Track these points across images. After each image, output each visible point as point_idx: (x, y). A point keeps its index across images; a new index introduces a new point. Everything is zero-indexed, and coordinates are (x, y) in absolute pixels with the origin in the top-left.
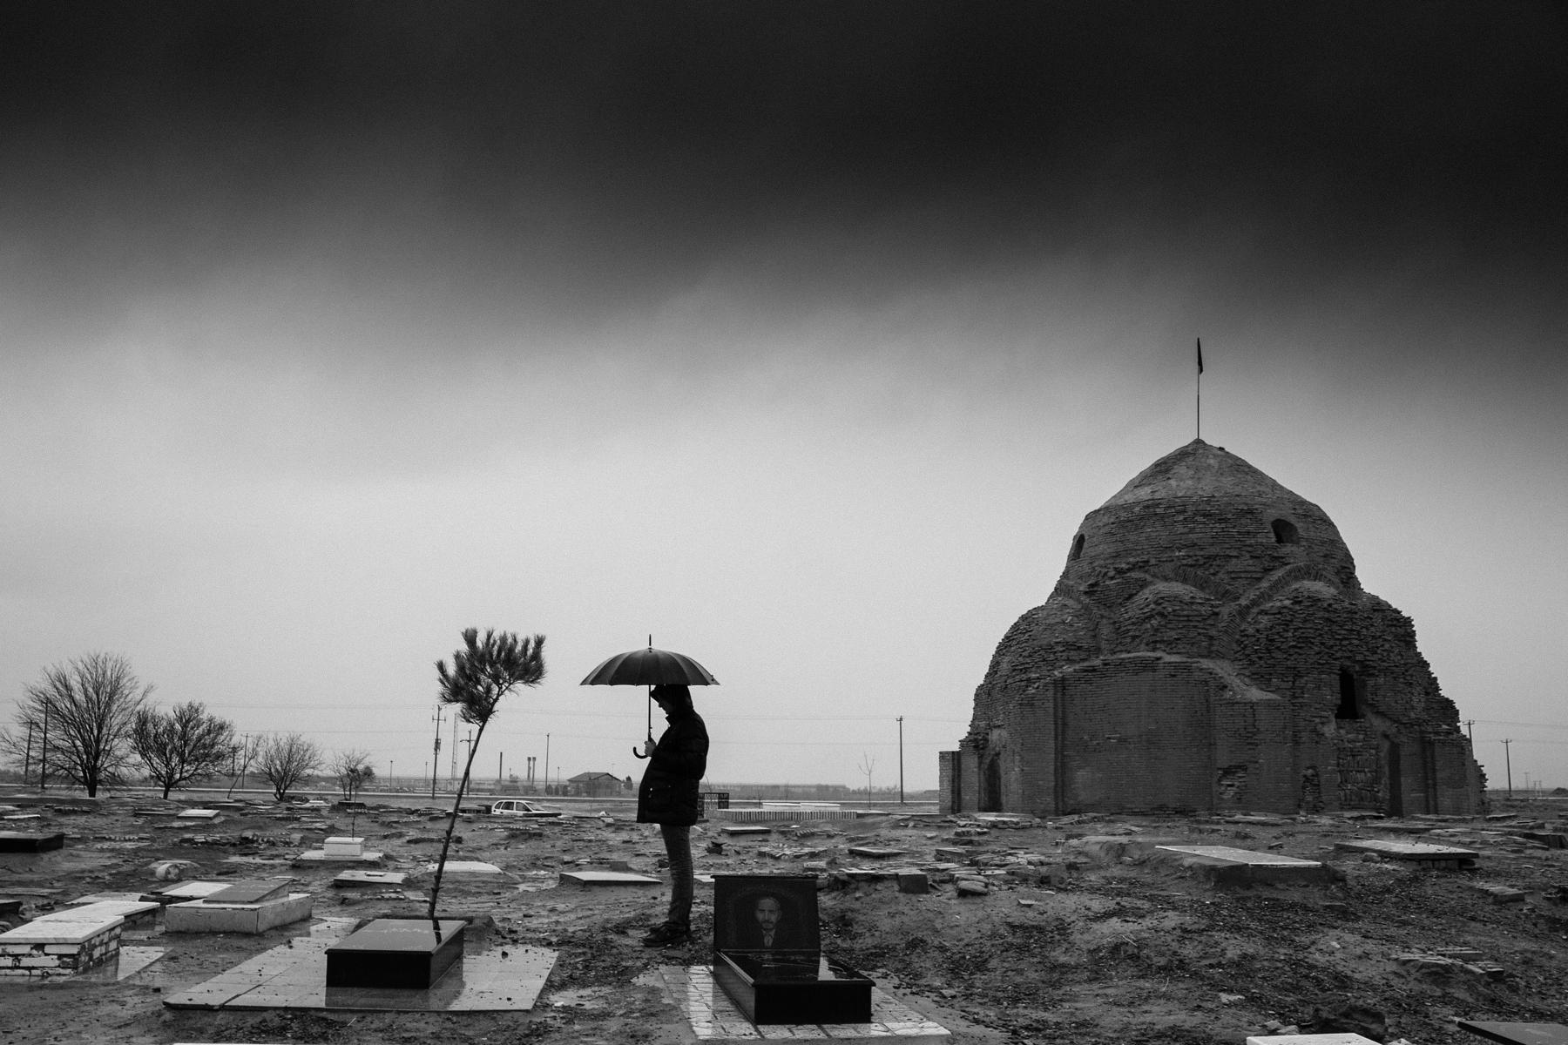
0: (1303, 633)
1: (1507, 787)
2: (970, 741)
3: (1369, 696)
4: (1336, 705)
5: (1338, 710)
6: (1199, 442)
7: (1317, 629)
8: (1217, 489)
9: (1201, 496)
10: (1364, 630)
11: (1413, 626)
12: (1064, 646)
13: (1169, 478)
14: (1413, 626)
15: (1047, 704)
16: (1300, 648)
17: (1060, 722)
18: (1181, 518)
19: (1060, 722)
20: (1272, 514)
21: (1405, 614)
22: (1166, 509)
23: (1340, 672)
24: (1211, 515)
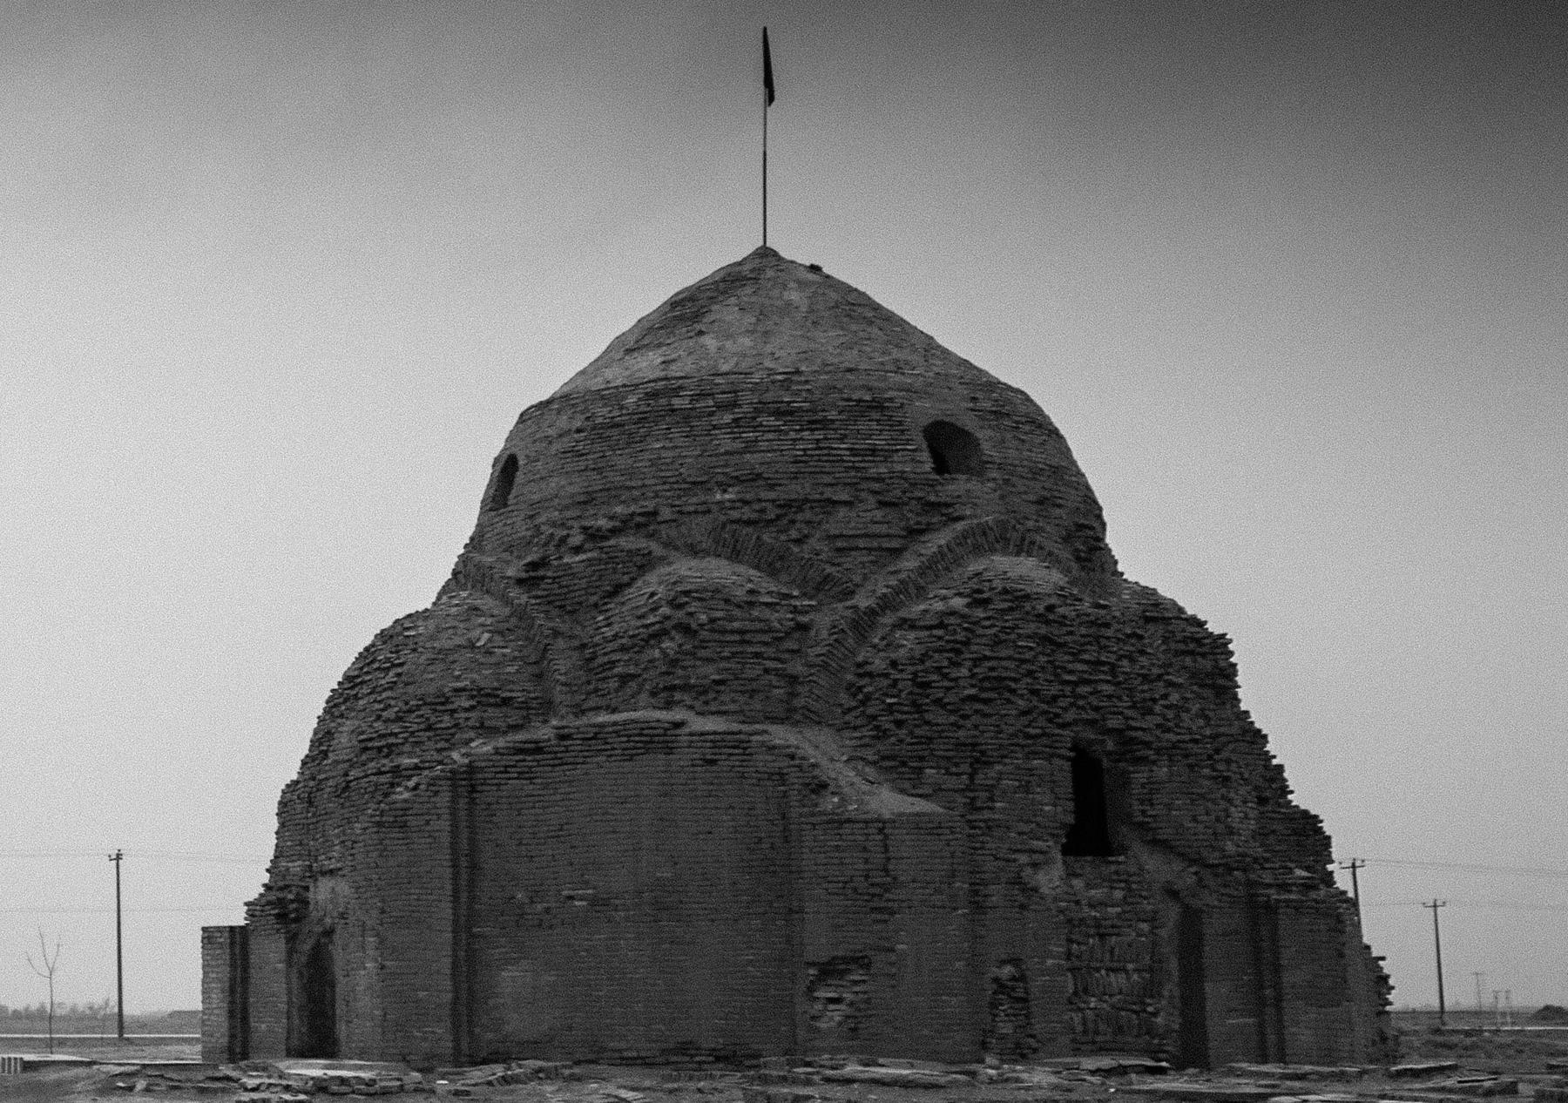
0: (992, 669)
3: (1137, 807)
6: (765, 254)
9: (771, 372)
10: (1125, 662)
12: (473, 697)
13: (701, 333)
16: (986, 701)
17: (464, 862)
18: (728, 418)
19: (464, 862)
20: (925, 411)
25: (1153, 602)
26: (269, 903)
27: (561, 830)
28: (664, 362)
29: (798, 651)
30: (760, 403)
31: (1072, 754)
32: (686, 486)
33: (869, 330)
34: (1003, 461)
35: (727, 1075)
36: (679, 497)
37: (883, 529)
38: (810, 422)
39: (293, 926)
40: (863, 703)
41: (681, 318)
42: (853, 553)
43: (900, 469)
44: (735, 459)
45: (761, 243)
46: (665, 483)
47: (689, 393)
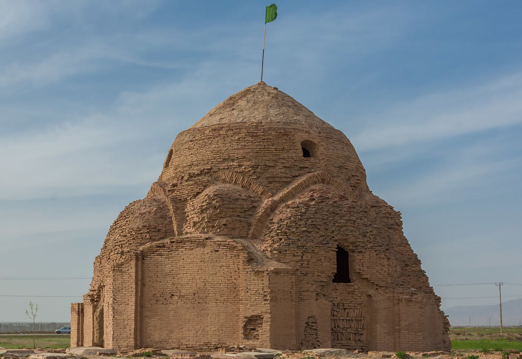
0: (312, 222)
1: (500, 324)
2: (89, 296)
3: (358, 267)
4: (333, 273)
5: (334, 276)
7: (323, 219)
8: (266, 117)
9: (253, 123)
10: (359, 220)
11: (401, 218)
13: (233, 109)
14: (401, 218)
15: (130, 271)
16: (309, 232)
17: (139, 283)
18: (237, 138)
19: (139, 283)
20: (300, 137)
21: (396, 209)
22: (227, 131)
23: (337, 250)
24: (257, 136)
25: (376, 201)
27: (170, 272)
28: (220, 119)
30: (247, 133)
32: (221, 160)
41: (228, 104)
42: (274, 183)
43: (291, 155)
44: (236, 151)
45: (259, 81)
46: (215, 159)
47: (225, 129)
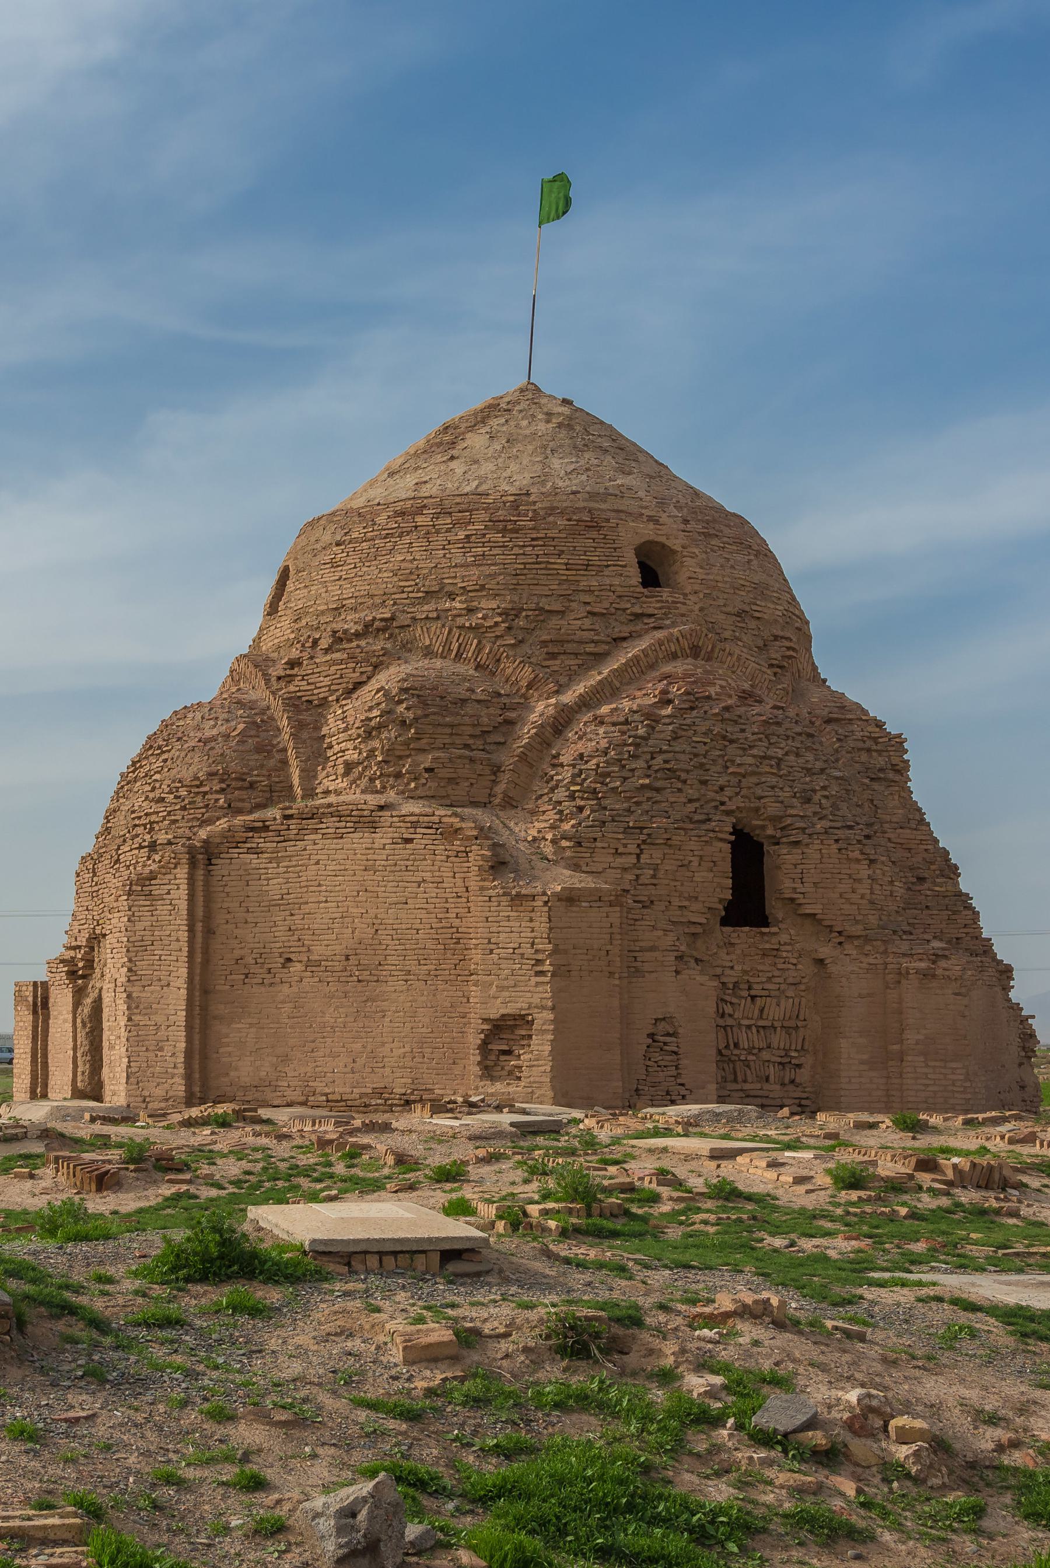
0: (666, 762)
9: (505, 494)
13: (452, 458)
16: (658, 790)
17: (199, 926)
18: (461, 535)
19: (199, 926)
26: (62, 961)
27: (282, 899)
29: (504, 743)
30: (490, 521)
31: (733, 838)
33: (602, 458)
34: (704, 577)
35: (741, 1151)
36: (413, 605)
37: (590, 635)
38: (533, 539)
39: (80, 982)
40: (552, 790)
43: (608, 582)
